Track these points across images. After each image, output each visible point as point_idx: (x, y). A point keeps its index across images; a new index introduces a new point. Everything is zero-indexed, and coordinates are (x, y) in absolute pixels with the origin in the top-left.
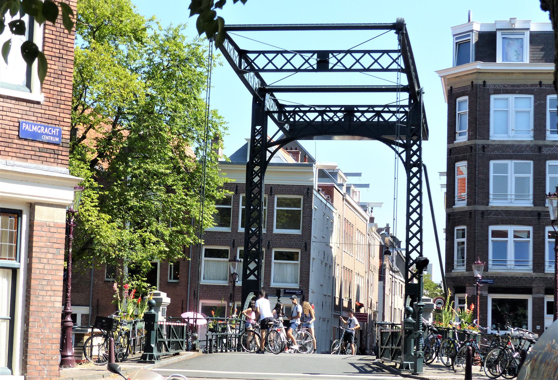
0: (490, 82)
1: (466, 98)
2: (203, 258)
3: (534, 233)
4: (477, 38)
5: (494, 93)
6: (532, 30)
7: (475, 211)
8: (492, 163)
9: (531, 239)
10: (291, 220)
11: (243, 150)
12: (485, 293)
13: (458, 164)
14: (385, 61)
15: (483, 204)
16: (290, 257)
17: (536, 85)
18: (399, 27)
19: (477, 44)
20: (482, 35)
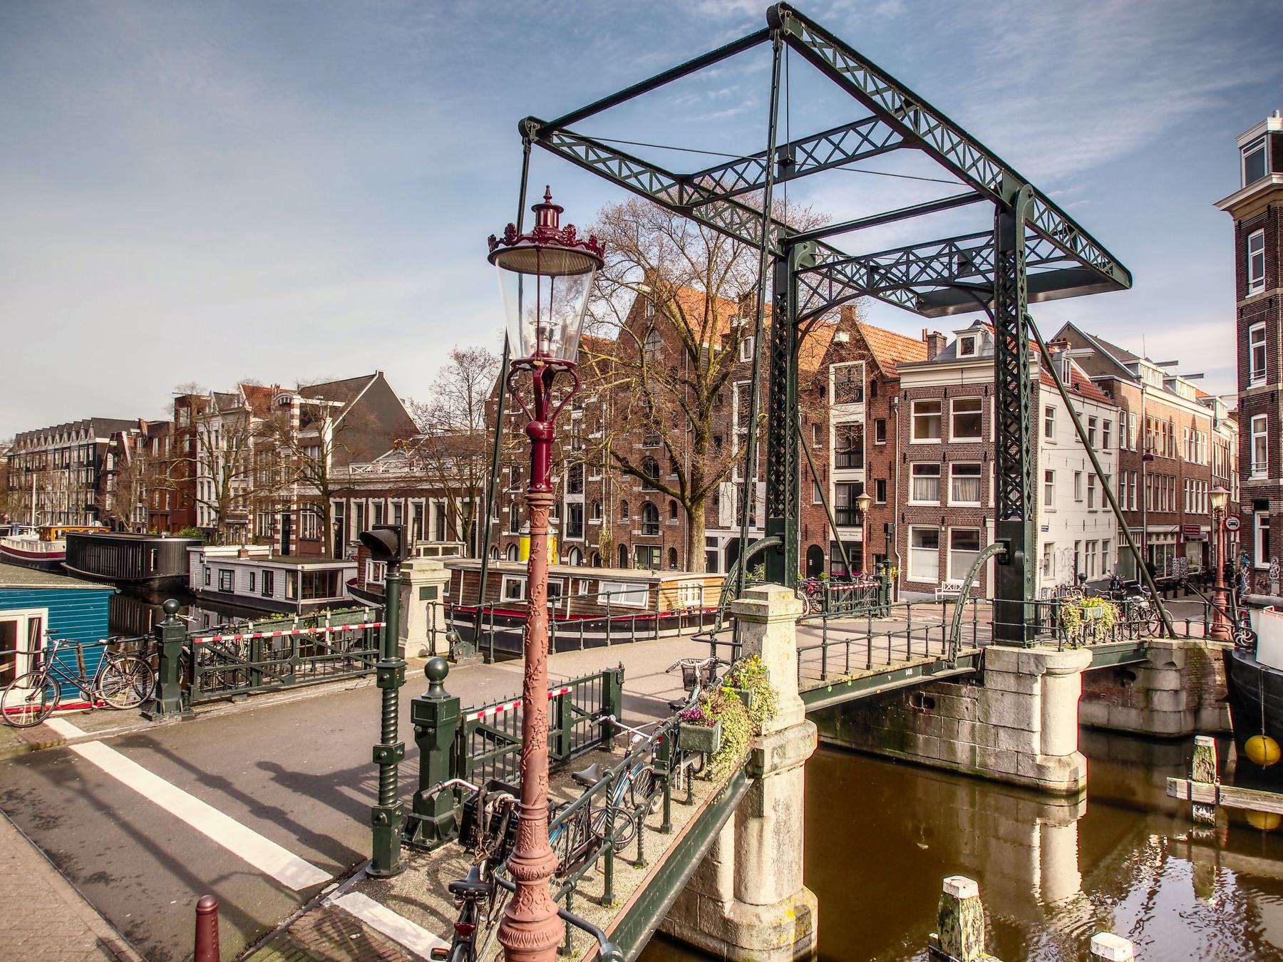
1: (1262, 231)
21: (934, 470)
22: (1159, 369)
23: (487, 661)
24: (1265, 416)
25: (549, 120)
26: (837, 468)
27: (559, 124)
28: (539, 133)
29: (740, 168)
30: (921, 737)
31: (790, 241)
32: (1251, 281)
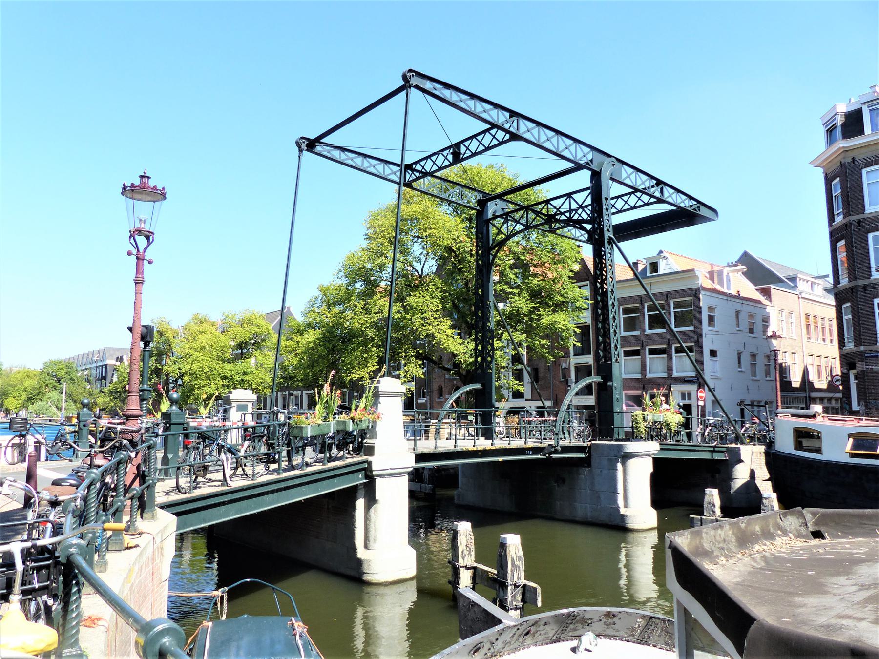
0: (859, 157)
1: (838, 179)
2: (648, 356)
4: (844, 119)
5: (865, 167)
7: (856, 286)
10: (681, 320)
15: (864, 278)
19: (843, 125)
21: (635, 353)
22: (816, 281)
25: (312, 138)
26: (575, 355)
27: (318, 140)
28: (307, 146)
29: (434, 158)
30: (558, 503)
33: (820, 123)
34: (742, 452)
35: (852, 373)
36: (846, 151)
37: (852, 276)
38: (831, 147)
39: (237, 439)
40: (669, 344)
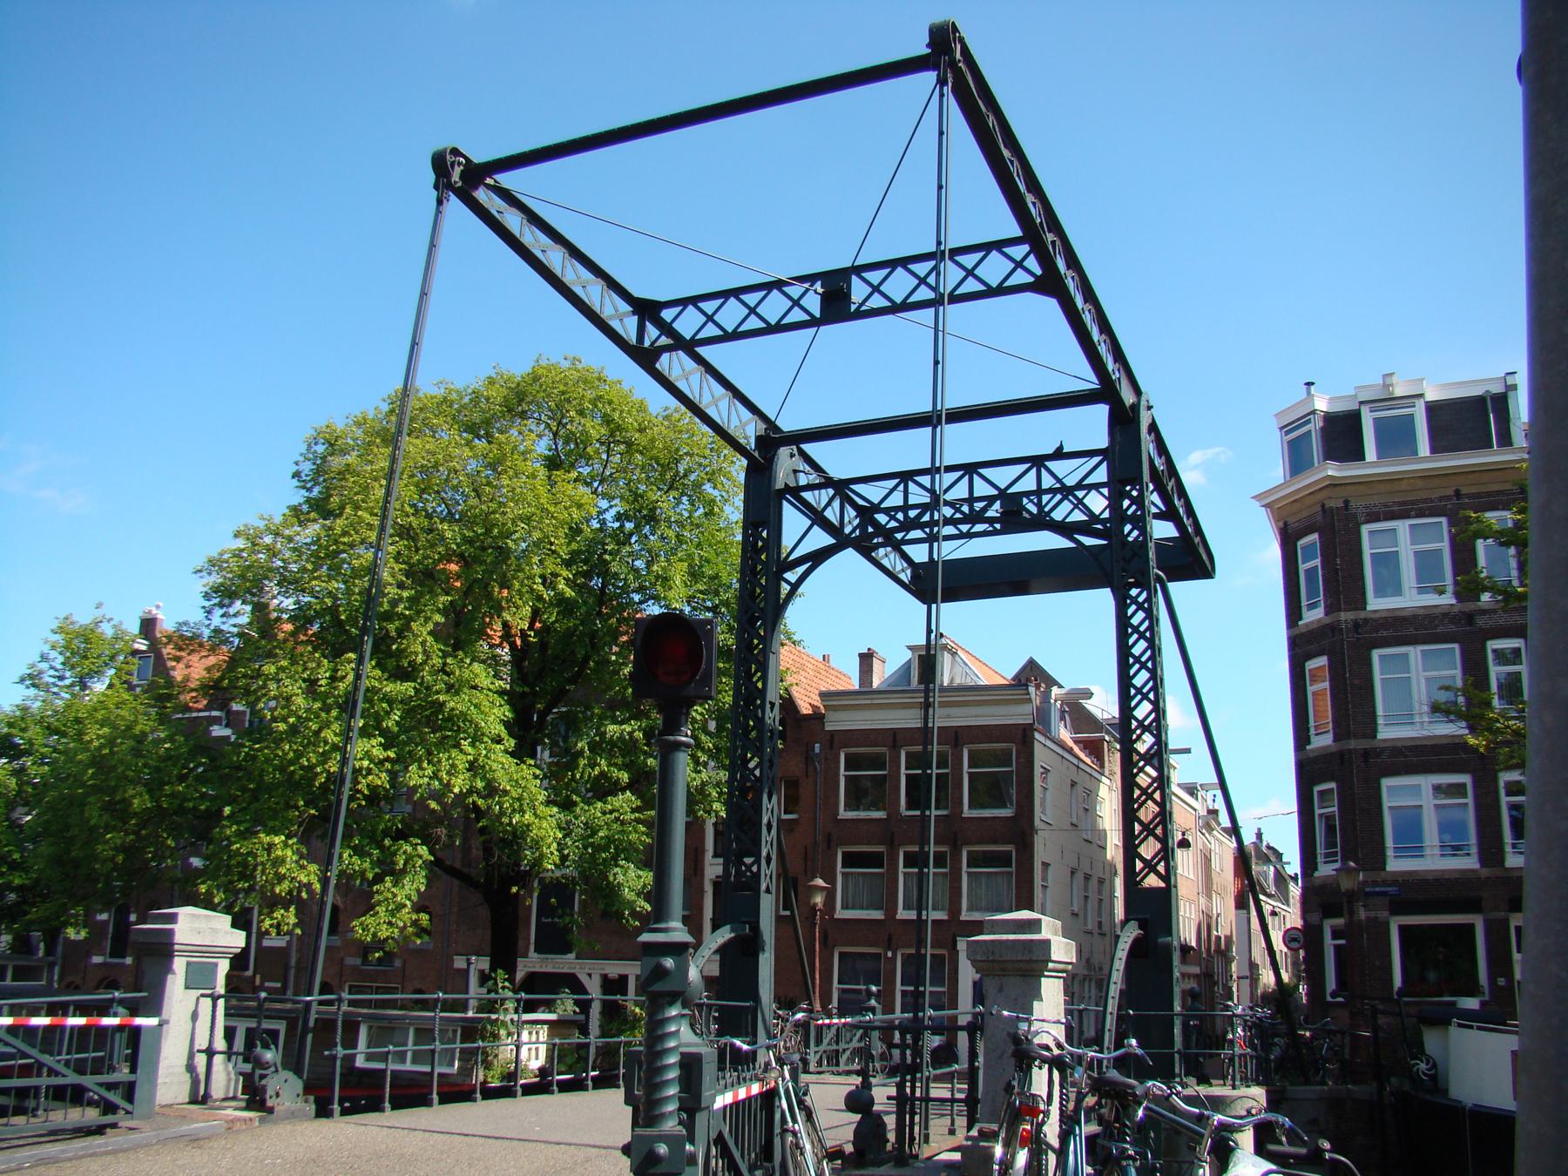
1: (1314, 537)
3: (1475, 787)
6: (1431, 396)
8: (1376, 654)
9: (1470, 800)
10: (990, 791)
11: (907, 666)
12: (1383, 914)
13: (1311, 665)
14: (994, 269)
15: (1365, 736)
16: (1002, 860)
17: (1448, 498)
18: (945, 53)
20: (1330, 419)
23: (323, 1111)
24: (1333, 785)
31: (772, 440)
32: (1304, 603)
33: (1273, 427)
34: (614, 1090)
35: (1328, 925)
36: (1334, 485)
37: (1342, 730)
38: (1299, 477)
39: (236, 1090)
40: (893, 847)
